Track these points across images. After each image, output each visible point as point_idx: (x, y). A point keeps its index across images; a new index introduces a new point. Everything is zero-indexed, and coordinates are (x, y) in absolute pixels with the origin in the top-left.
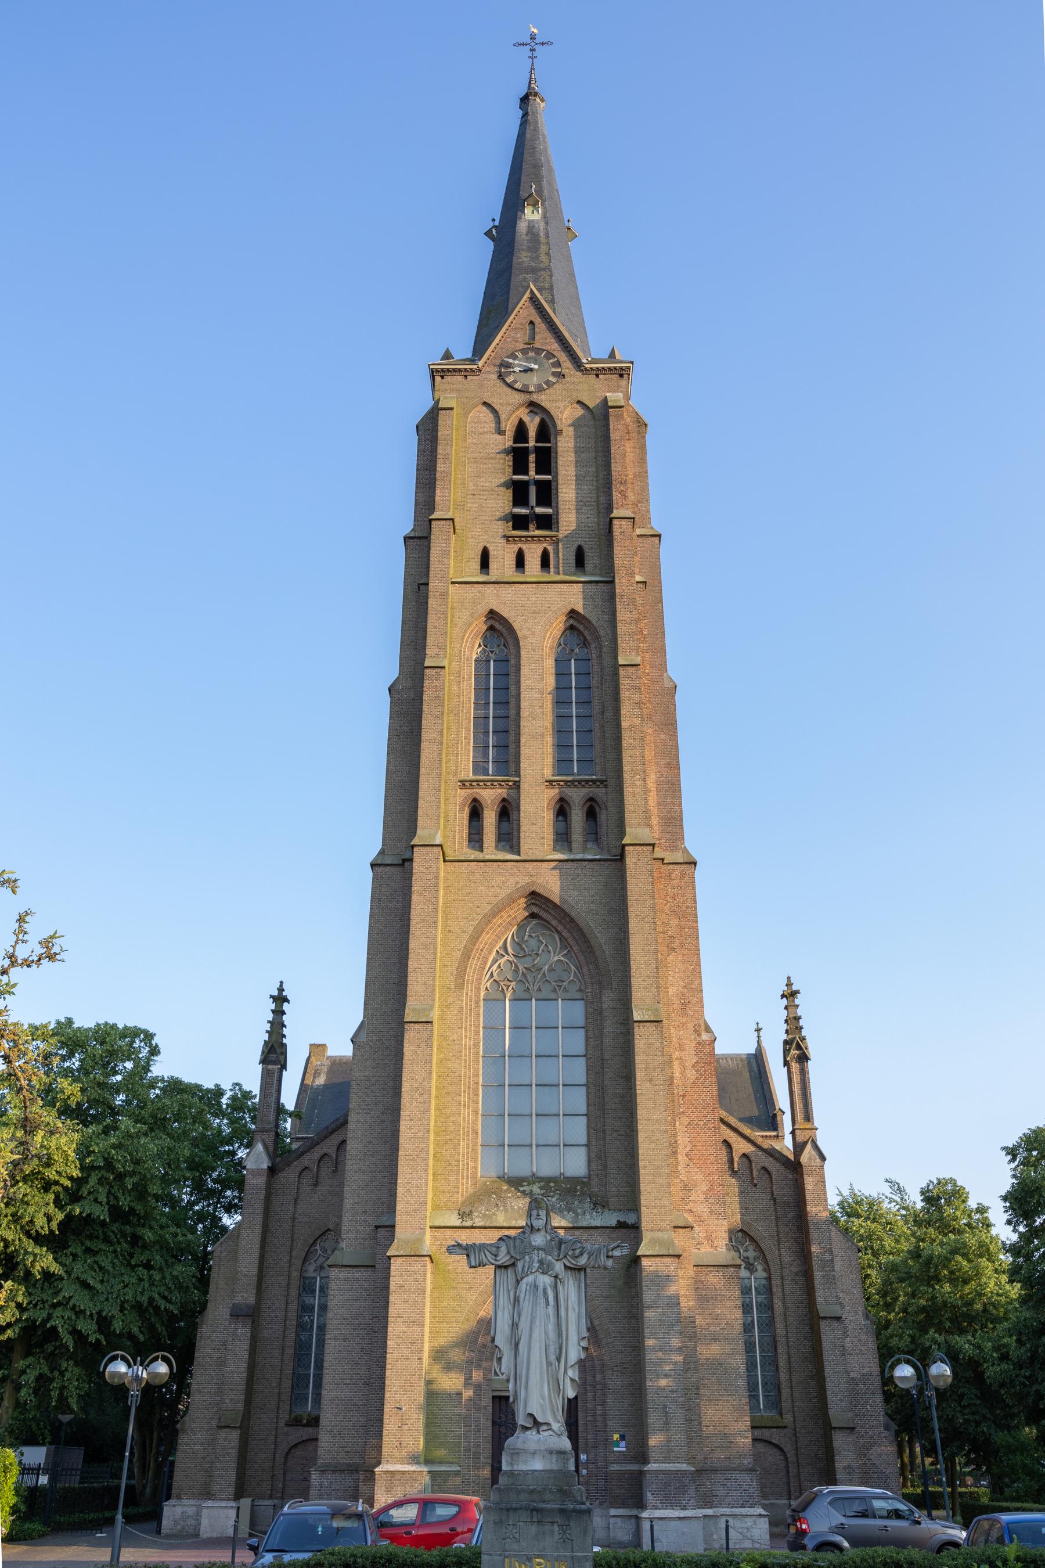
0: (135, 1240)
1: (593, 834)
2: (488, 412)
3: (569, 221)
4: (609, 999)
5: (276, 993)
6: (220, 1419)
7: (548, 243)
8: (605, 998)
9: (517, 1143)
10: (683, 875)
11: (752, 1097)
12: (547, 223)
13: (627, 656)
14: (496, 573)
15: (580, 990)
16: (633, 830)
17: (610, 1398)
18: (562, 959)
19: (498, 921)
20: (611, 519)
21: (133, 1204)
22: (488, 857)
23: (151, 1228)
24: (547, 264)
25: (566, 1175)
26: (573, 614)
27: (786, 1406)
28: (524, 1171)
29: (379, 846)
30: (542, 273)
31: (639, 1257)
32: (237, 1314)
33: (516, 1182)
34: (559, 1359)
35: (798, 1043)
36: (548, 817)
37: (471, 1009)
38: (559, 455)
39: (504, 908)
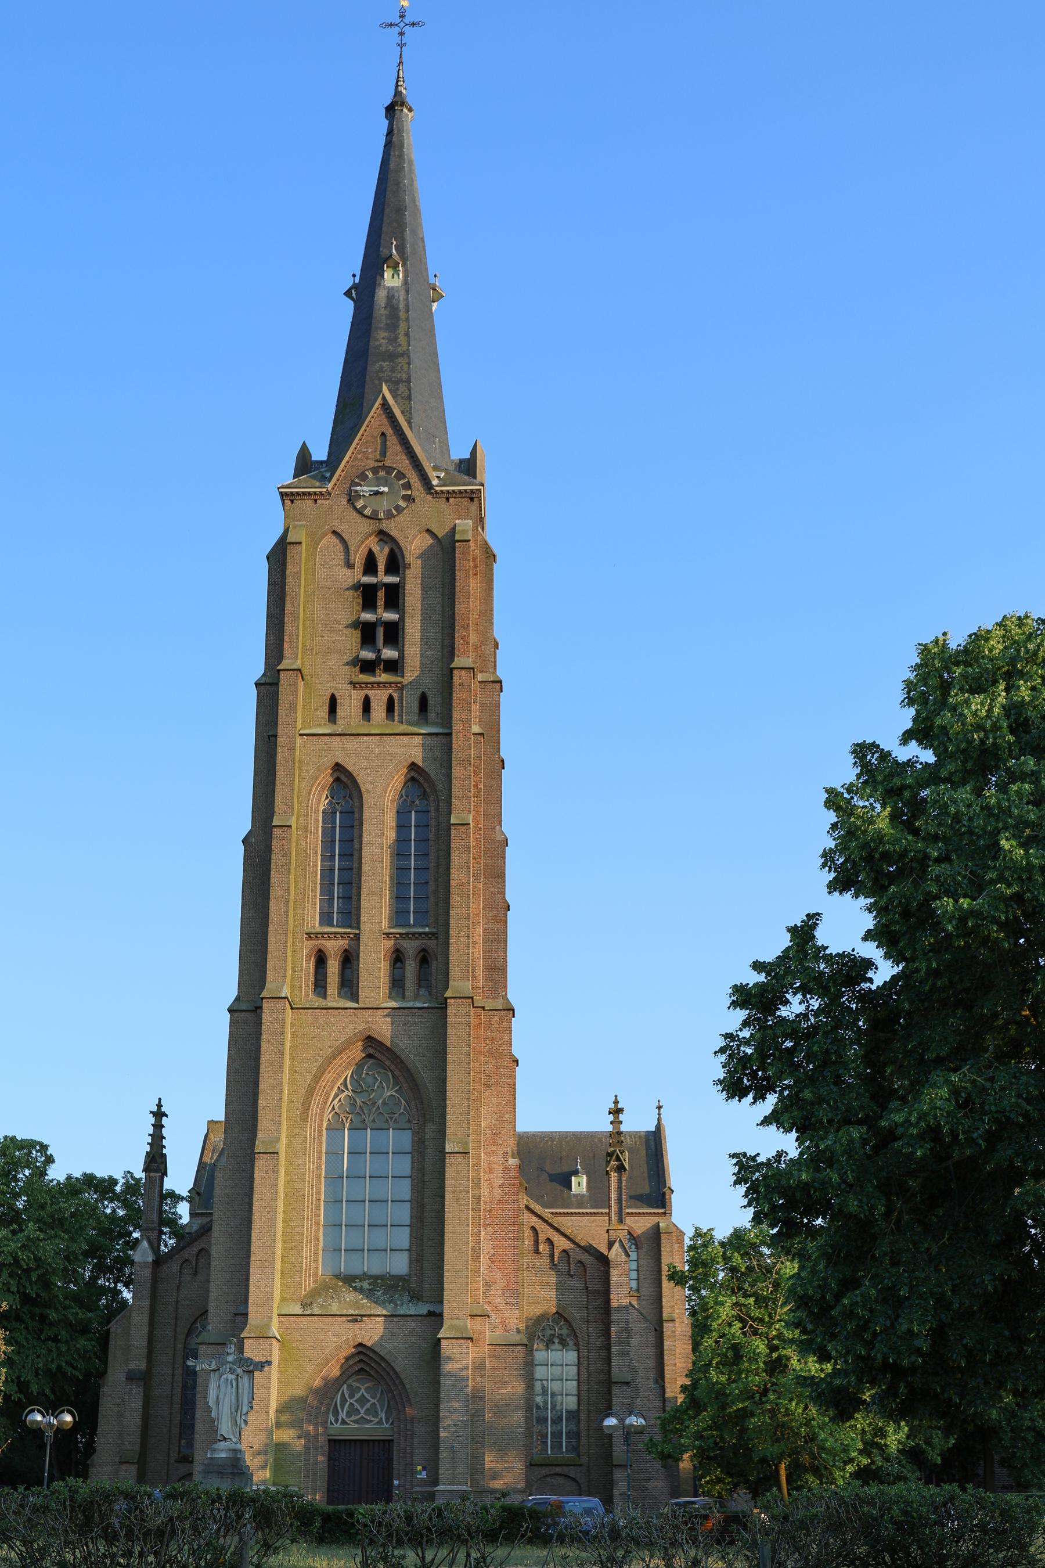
0: (43, 1318)
1: (423, 980)
2: (337, 541)
3: (435, 276)
4: (430, 1129)
5: (155, 1109)
6: (121, 1457)
7: (407, 320)
8: (427, 1131)
9: (352, 1248)
10: (502, 1020)
11: (646, 1175)
12: (407, 292)
13: (459, 813)
14: (343, 722)
15: (409, 1121)
16: (455, 983)
17: (416, 1441)
18: (394, 1094)
19: (338, 1061)
20: (452, 670)
21: (39, 1291)
22: (330, 1005)
23: (56, 1309)
24: (405, 348)
25: (392, 1274)
26: (413, 766)
27: (583, 1449)
28: (357, 1271)
29: (235, 993)
30: (400, 360)
31: (439, 1340)
32: (131, 1377)
33: (349, 1280)
34: (237, 1412)
35: (618, 1155)
36: (384, 968)
37: (314, 1138)
38: (407, 591)
39: (344, 1050)
